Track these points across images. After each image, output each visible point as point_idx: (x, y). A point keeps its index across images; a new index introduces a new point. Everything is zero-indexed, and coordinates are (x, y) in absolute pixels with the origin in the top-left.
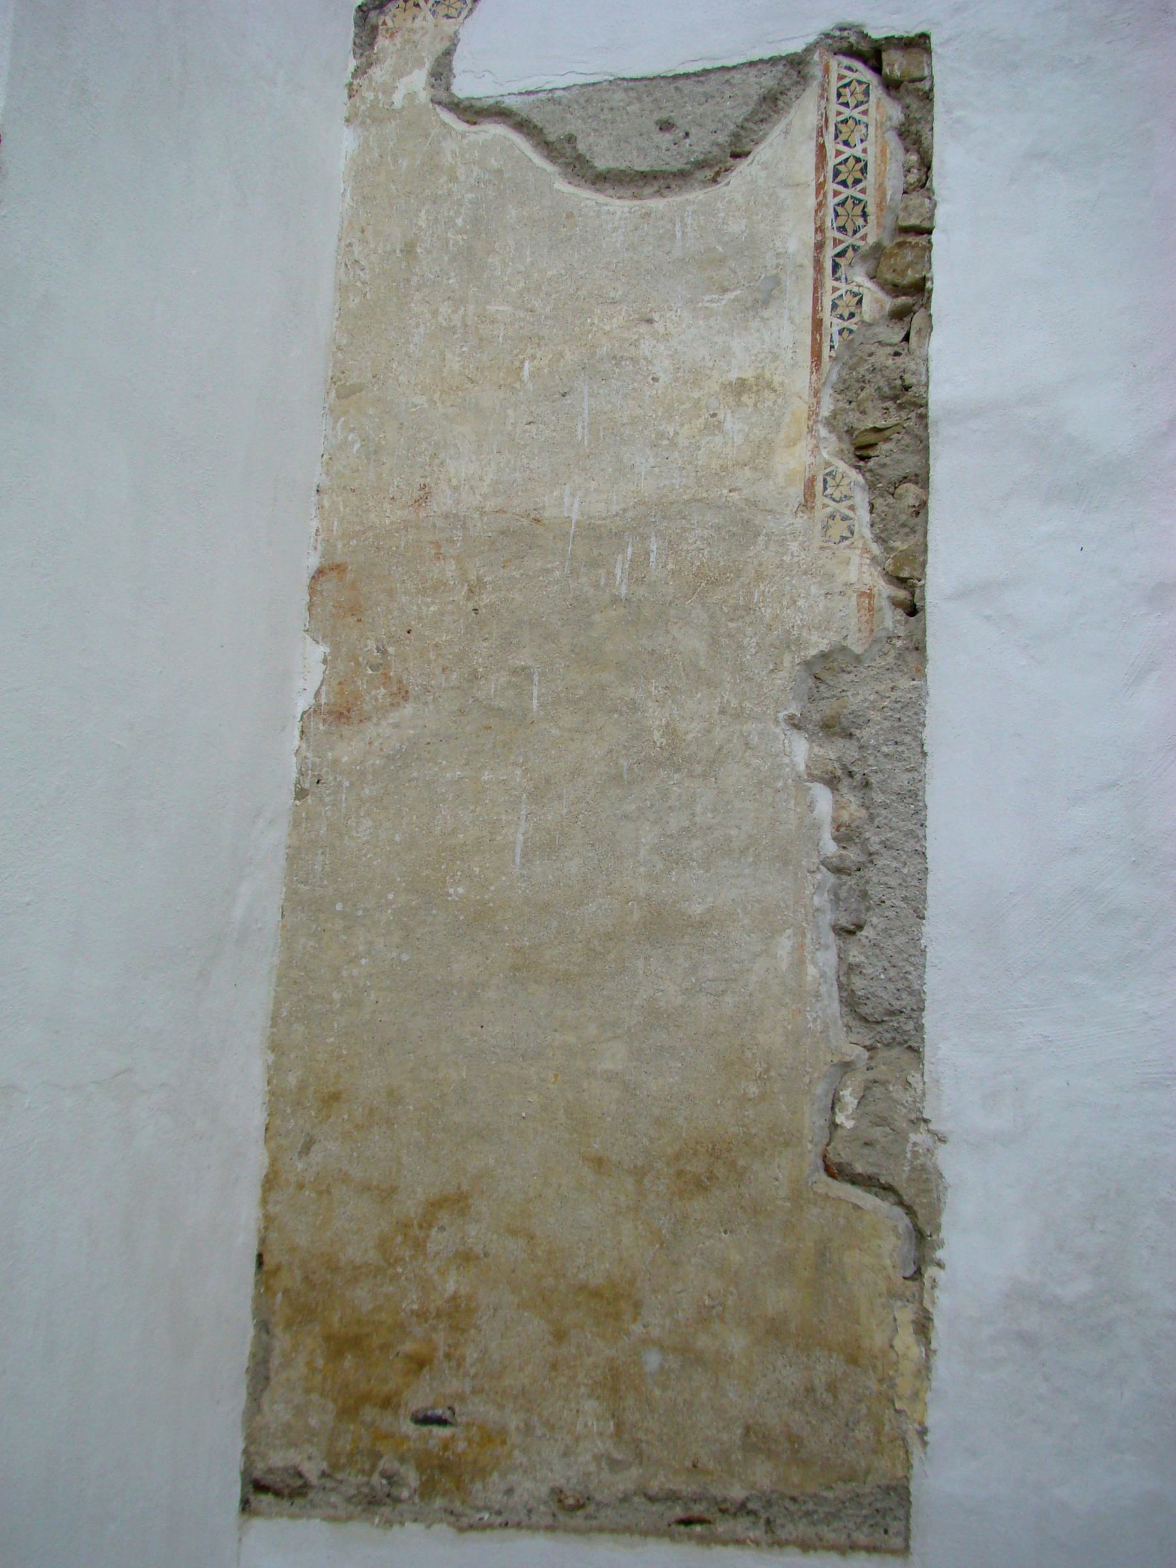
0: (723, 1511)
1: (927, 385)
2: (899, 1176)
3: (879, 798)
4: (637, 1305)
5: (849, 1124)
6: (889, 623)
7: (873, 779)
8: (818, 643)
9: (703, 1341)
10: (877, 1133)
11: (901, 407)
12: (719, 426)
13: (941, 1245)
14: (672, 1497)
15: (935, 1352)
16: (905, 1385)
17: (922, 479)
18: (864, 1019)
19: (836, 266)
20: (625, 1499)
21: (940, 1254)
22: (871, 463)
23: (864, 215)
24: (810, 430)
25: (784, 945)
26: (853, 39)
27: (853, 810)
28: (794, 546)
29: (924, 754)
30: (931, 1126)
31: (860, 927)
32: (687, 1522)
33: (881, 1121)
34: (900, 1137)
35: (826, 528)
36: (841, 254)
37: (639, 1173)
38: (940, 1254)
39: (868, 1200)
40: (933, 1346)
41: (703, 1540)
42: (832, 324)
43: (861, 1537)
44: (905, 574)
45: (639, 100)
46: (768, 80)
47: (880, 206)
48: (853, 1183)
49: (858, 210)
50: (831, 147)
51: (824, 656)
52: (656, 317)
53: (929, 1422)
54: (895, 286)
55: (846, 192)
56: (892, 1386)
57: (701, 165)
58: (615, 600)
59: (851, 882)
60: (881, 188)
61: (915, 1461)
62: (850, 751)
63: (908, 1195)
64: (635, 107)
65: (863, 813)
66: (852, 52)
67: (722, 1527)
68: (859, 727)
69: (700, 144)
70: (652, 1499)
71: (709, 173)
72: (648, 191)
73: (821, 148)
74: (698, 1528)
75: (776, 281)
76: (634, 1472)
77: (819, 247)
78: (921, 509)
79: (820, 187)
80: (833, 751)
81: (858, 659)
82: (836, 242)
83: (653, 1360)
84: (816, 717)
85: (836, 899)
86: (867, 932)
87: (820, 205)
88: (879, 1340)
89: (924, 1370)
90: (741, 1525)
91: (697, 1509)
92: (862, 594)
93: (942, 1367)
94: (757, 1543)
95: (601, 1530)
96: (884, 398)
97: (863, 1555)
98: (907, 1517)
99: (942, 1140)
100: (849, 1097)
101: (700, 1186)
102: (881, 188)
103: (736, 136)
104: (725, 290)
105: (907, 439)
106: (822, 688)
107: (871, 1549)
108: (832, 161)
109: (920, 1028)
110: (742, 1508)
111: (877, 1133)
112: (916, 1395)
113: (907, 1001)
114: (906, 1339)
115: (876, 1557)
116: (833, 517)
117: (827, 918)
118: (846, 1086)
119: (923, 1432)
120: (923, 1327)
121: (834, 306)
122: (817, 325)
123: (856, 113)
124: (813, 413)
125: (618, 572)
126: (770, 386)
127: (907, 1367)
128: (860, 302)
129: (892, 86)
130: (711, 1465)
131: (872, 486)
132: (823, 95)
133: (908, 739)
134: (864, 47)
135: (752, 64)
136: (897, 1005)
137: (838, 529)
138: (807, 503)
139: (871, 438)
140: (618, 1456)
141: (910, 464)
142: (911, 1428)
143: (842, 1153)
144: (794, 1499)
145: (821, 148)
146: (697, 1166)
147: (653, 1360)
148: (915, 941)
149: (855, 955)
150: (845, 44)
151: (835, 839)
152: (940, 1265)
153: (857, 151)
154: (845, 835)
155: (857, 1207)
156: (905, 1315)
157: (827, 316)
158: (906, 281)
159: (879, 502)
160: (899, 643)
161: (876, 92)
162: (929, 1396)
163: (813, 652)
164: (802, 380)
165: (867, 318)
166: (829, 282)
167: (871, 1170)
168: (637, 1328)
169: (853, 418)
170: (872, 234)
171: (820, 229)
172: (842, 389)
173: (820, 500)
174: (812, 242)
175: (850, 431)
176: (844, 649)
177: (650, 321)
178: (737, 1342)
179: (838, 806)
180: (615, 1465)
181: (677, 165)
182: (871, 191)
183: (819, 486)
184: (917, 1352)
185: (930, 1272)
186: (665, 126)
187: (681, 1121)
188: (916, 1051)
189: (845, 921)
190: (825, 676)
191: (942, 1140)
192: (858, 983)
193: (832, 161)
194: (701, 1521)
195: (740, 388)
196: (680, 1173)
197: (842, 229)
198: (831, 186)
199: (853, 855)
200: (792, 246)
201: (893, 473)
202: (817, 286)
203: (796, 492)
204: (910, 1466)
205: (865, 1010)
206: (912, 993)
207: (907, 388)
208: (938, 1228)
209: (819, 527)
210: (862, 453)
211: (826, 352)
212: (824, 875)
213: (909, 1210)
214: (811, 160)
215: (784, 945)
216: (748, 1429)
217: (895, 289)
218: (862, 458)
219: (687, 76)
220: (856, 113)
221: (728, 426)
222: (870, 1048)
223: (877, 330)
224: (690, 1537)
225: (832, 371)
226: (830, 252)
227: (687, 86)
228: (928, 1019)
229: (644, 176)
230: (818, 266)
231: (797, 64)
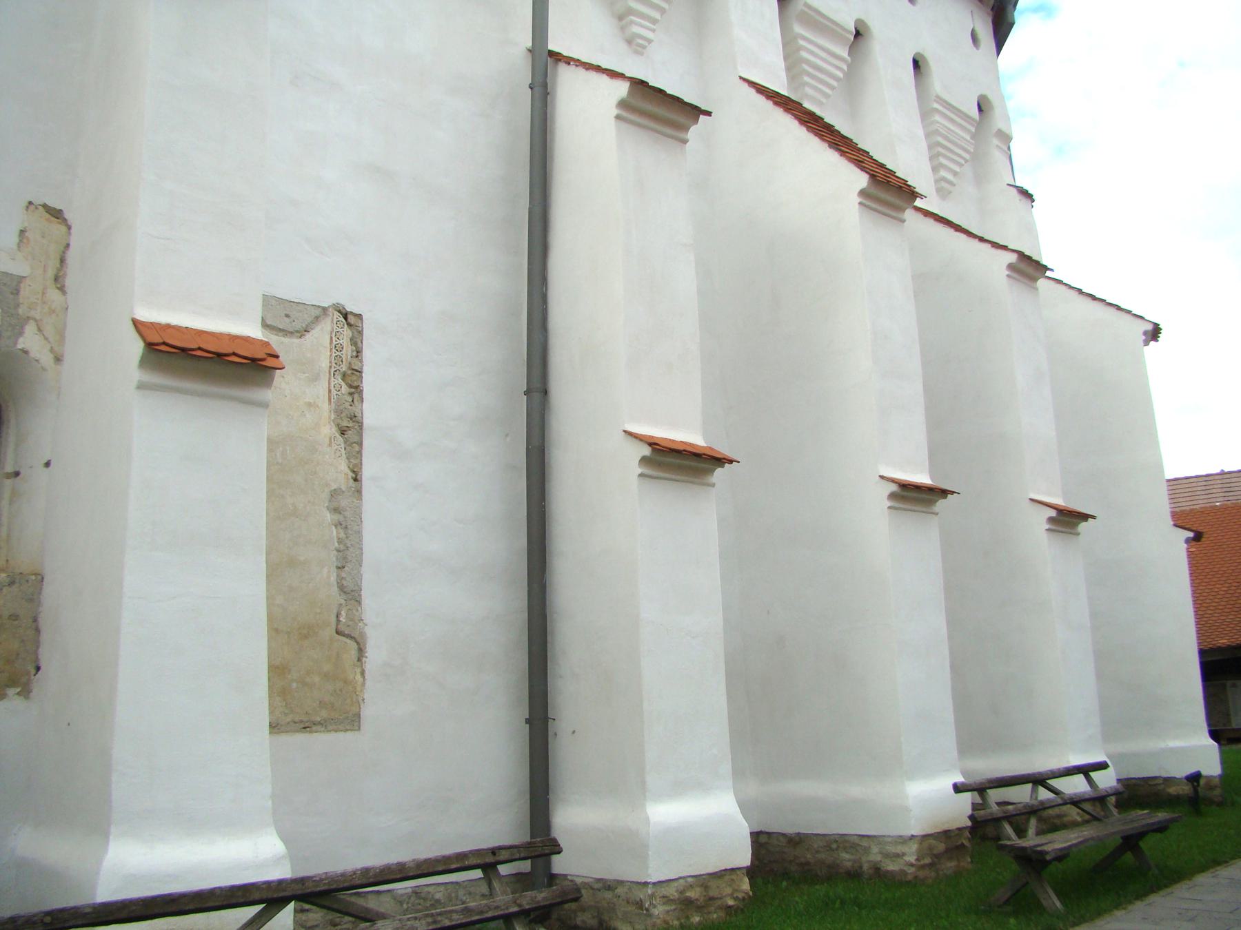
0: (314, 724)
1: (362, 417)
2: (356, 634)
3: (350, 532)
4: (290, 670)
5: (344, 621)
6: (351, 483)
7: (349, 527)
8: (334, 486)
9: (308, 680)
10: (350, 623)
11: (354, 422)
12: (305, 415)
13: (366, 652)
14: (301, 721)
15: (1222, 470)
16: (359, 689)
17: (360, 444)
18: (345, 592)
19: (334, 374)
20: (288, 723)
21: (367, 654)
22: (346, 436)
23: (342, 361)
24: (329, 422)
25: (325, 570)
26: (341, 308)
27: (342, 535)
28: (327, 457)
29: (362, 522)
30: (364, 621)
31: (344, 567)
32: (304, 728)
33: (352, 620)
34: (357, 624)
35: (335, 453)
36: (336, 371)
37: (288, 633)
38: (367, 654)
39: (348, 641)
40: (366, 678)
41: (311, 732)
42: (334, 392)
43: (348, 727)
44: (355, 470)
45: (280, 305)
46: (318, 312)
47: (346, 360)
48: (344, 636)
49: (340, 359)
50: (334, 338)
51: (335, 490)
52: (285, 376)
53: (365, 697)
54: (351, 385)
55: (338, 353)
56: (355, 689)
57: (297, 332)
58: (277, 463)
59: (341, 554)
60: (347, 355)
61: (362, 707)
62: (341, 518)
63: (358, 640)
64: (278, 307)
65: (345, 536)
66: (340, 312)
67: (314, 728)
68: (344, 511)
69: (298, 325)
70: (295, 723)
71: (299, 335)
72: (280, 334)
73: (331, 338)
74: (308, 729)
75: (318, 374)
76: (291, 716)
77: (330, 367)
78: (360, 453)
79: (331, 349)
80: (336, 517)
81: (343, 492)
82: (335, 367)
83: (294, 685)
84: (332, 507)
85: (337, 559)
86: (346, 568)
87: (331, 355)
88: (351, 677)
89: (363, 684)
90: (319, 728)
91: (307, 725)
92: (345, 474)
93: (368, 683)
94: (324, 731)
95: (283, 732)
96: (348, 417)
97: (350, 732)
98: (360, 721)
99: (366, 625)
100: (343, 613)
101: (306, 637)
102: (347, 355)
103: (307, 326)
104: (304, 373)
105: (355, 432)
106: (333, 499)
107: (351, 730)
108: (334, 343)
109: (360, 595)
110: (320, 723)
111: (350, 623)
112: (361, 691)
113: (356, 588)
114: (358, 677)
115: (353, 732)
116: (336, 450)
117: (335, 564)
118: (342, 610)
119: (363, 700)
120: (363, 673)
121: (334, 387)
122: (330, 391)
123: (341, 330)
124: (330, 418)
125: (278, 454)
126: (318, 406)
127: (359, 683)
128: (341, 387)
129: (349, 325)
130: (311, 712)
131: (345, 443)
132: (332, 322)
133: (357, 517)
134: (344, 311)
135: (313, 305)
136: (354, 589)
137: (338, 454)
138: (330, 445)
139: (345, 429)
140: (286, 712)
141: (356, 438)
142: (360, 699)
143: (342, 628)
144: (332, 719)
145: (331, 338)
146: (305, 632)
147: (294, 685)
148: (359, 572)
149: (344, 575)
150: (338, 309)
151: (338, 542)
152: (366, 657)
153: (341, 342)
154: (340, 541)
155: (346, 642)
156: (358, 670)
157: (332, 388)
158: (354, 385)
159: (347, 448)
160: (353, 489)
161: (346, 326)
162: (365, 691)
163: (333, 488)
164: (326, 406)
165: (343, 393)
166: (332, 379)
167: (349, 633)
168: (290, 676)
169: (339, 421)
170: (344, 368)
171: (330, 362)
172: (336, 411)
173: (333, 444)
174: (328, 365)
175: (338, 425)
176: (340, 489)
177: (283, 377)
178: (317, 679)
179: (338, 533)
180: (286, 714)
181: (291, 330)
182: (344, 355)
183: (333, 441)
184: (361, 679)
185: (364, 659)
186: (287, 316)
187: (299, 619)
188: (359, 603)
189: (340, 565)
190: (335, 495)
191: (366, 625)
192: (345, 583)
193: (334, 343)
194: (308, 727)
195: (310, 405)
196: (300, 634)
197: (336, 364)
198: (334, 350)
199: (342, 547)
200: (324, 365)
201: (351, 440)
202: (330, 379)
203: (327, 441)
204: (360, 708)
205: (345, 590)
206: (358, 586)
207: (355, 417)
208: (366, 648)
209: (333, 452)
210: (343, 433)
211: (332, 400)
212: (335, 552)
213: (358, 643)
214: (328, 341)
215: (325, 570)
216: (320, 702)
217: (351, 386)
218: (343, 434)
219: (294, 302)
220: (341, 330)
221: (307, 416)
222: (345, 600)
223: (346, 396)
224: (307, 731)
225: (333, 405)
226: (333, 370)
227: (294, 305)
228: (363, 593)
229: (280, 329)
230: (330, 372)
231: (325, 309)
